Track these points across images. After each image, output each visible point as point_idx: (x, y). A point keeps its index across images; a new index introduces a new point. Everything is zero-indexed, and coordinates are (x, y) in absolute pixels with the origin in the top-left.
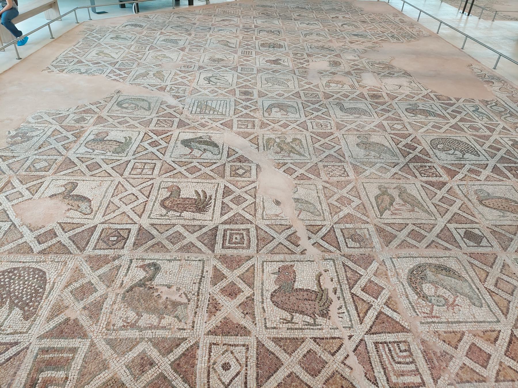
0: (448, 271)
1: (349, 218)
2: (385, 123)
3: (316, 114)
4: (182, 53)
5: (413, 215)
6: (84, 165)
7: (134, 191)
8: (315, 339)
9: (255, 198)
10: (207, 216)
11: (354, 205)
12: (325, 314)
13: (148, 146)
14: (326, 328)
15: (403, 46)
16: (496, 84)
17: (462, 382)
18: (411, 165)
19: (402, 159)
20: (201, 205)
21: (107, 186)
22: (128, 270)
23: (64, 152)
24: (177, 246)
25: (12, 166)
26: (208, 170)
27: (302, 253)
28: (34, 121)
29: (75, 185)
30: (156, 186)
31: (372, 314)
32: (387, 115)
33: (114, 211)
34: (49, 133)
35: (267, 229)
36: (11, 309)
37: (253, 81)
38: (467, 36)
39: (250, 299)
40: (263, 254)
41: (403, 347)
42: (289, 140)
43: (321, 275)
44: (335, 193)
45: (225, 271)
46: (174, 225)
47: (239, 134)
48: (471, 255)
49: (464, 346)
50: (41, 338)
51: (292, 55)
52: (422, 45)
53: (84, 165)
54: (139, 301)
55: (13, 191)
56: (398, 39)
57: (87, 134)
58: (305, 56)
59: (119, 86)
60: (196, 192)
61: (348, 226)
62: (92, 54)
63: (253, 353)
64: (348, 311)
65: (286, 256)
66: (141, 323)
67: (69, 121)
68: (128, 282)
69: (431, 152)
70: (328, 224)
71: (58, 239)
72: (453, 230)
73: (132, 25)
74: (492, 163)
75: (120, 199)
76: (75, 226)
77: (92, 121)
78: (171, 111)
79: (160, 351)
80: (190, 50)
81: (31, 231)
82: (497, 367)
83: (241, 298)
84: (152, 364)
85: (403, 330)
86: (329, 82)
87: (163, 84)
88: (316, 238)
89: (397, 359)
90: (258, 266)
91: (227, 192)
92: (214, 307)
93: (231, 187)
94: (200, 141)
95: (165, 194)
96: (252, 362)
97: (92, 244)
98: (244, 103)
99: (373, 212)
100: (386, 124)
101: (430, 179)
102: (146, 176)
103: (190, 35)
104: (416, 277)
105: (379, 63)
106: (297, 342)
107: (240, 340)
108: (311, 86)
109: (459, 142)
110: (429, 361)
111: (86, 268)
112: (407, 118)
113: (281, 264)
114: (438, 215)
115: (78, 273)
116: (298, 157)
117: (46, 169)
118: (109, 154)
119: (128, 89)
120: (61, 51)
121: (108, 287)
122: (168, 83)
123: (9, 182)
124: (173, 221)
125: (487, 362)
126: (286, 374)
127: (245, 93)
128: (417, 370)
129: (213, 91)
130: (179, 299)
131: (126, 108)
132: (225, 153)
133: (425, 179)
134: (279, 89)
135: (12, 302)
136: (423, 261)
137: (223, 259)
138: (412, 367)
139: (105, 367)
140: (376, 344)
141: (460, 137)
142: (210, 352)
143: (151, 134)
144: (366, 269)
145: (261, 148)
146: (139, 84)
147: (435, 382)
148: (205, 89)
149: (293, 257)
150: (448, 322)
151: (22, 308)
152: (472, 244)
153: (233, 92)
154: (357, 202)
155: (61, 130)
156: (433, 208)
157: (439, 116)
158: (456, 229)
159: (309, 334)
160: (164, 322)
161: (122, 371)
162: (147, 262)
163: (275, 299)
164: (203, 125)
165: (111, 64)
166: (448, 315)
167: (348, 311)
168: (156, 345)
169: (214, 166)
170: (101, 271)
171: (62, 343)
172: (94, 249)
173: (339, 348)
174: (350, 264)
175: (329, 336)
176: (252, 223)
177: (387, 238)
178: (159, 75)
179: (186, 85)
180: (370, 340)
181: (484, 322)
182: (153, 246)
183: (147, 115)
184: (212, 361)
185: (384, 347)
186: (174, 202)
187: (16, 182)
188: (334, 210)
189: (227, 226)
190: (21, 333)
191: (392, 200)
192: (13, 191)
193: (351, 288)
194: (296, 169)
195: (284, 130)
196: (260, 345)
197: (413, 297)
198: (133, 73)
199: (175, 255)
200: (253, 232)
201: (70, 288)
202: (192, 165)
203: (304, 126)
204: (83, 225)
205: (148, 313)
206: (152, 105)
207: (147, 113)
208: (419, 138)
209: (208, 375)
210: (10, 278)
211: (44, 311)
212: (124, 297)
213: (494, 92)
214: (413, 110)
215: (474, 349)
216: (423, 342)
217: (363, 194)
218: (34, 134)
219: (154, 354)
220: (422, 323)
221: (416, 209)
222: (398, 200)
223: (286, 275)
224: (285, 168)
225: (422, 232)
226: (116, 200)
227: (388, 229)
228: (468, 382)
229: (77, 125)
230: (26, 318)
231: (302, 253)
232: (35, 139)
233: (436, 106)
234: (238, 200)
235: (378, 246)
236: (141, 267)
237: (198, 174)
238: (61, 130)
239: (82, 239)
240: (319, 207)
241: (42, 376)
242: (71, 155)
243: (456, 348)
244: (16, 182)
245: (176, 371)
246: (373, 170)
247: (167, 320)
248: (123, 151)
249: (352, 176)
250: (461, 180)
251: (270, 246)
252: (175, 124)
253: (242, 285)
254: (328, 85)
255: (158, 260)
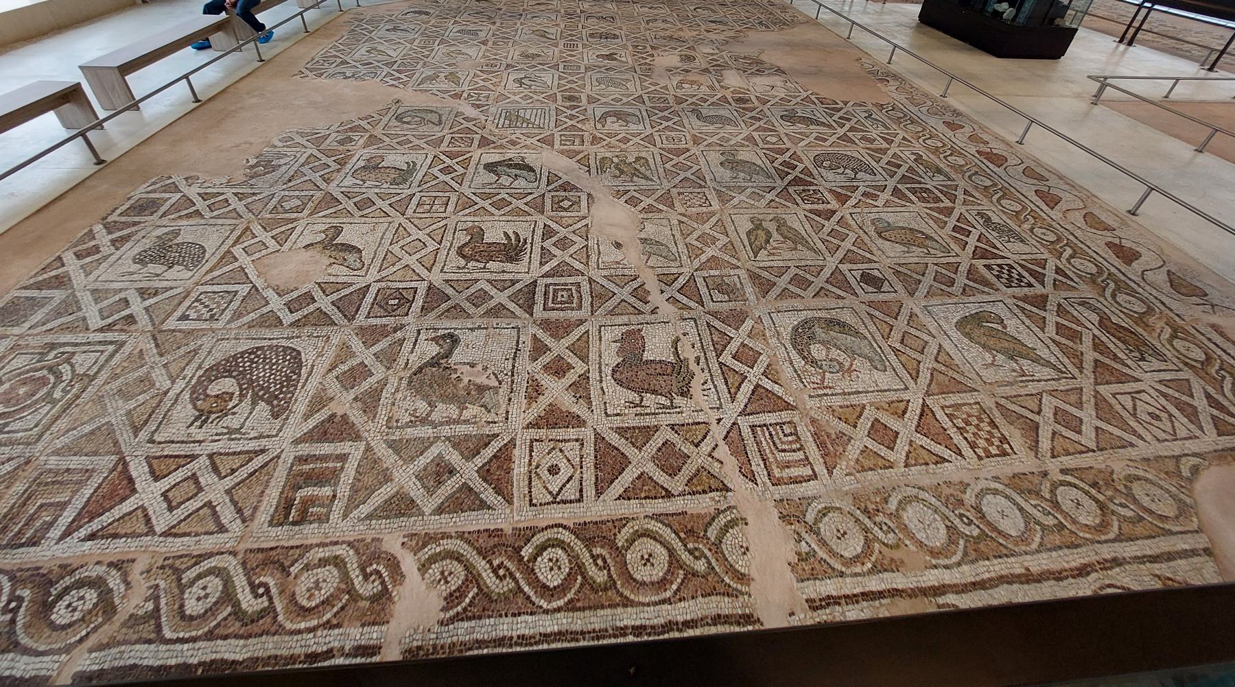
0: (842, 326)
1: (713, 262)
2: (756, 134)
3: (665, 124)
4: (484, 48)
5: (796, 255)
6: (351, 202)
7: (421, 235)
8: (672, 426)
9: (587, 240)
10: (522, 266)
11: (719, 244)
12: (685, 393)
13: (438, 174)
14: (686, 410)
15: (774, 36)
16: (892, 82)
17: (864, 470)
18: (791, 190)
19: (779, 181)
20: (512, 251)
21: (383, 230)
22: (415, 345)
23: (323, 185)
24: (482, 310)
25: (251, 207)
26: (520, 204)
27: (653, 312)
28: (281, 144)
29: (338, 231)
30: (451, 227)
31: (747, 388)
32: (758, 124)
33: (393, 265)
34: (302, 160)
35: (605, 282)
36: (254, 403)
37: (580, 82)
38: (854, 23)
39: (585, 377)
40: (601, 316)
41: (787, 430)
42: (631, 159)
43: (678, 340)
44: (695, 229)
45: (549, 341)
46: (477, 281)
47: (562, 152)
48: (870, 304)
49: (865, 424)
50: (297, 442)
51: (631, 48)
52: (797, 34)
53: (351, 202)
54: (431, 386)
55: (253, 241)
56: (767, 27)
57: (354, 159)
58: (649, 49)
59: (399, 93)
60: (505, 233)
61: (712, 272)
62: (362, 52)
63: (589, 449)
64: (715, 387)
65: (632, 317)
66: (435, 417)
67: (330, 143)
68: (415, 361)
69: (815, 172)
70: (686, 270)
71: (316, 305)
72: (846, 272)
73: (415, 12)
74: (891, 183)
75: (402, 248)
76: (340, 286)
77: (362, 141)
78: (470, 125)
79: (462, 454)
80: (494, 43)
81: (280, 296)
82: (906, 448)
83: (571, 377)
84: (452, 472)
85: (788, 407)
86: (681, 82)
87: (458, 90)
88: (672, 291)
89: (779, 446)
90: (594, 331)
91: (548, 233)
92: (535, 391)
93: (554, 226)
94: (509, 164)
95: (463, 238)
96: (589, 462)
97: (364, 310)
98: (569, 112)
99: (745, 253)
100: (757, 137)
101: (816, 206)
102: (436, 215)
103: (494, 23)
104: (802, 337)
105: (745, 58)
106: (648, 432)
107: (572, 433)
108: (657, 88)
109: (850, 158)
110: (821, 445)
111: (356, 344)
112: (784, 128)
113: (624, 329)
114: (827, 254)
115: (345, 351)
116: (643, 182)
117: (298, 210)
118: (385, 186)
119: (411, 98)
120: (317, 49)
121: (388, 369)
122: (465, 87)
123: (248, 228)
124: (475, 276)
125: (895, 442)
126: (635, 475)
127: (570, 98)
128: (807, 458)
129: (525, 97)
130: (486, 382)
131: (408, 123)
132: (544, 179)
133: (808, 207)
134: (615, 92)
135: (255, 395)
136: (810, 314)
137: (545, 324)
138: (800, 455)
139: (388, 479)
140: (753, 427)
141: (849, 151)
142: (531, 451)
143: (443, 157)
144: (737, 329)
145: (593, 171)
146: (426, 91)
147: (830, 473)
148: (515, 94)
149: (640, 317)
150: (844, 394)
151: (269, 403)
152: (870, 289)
153: (553, 97)
154: (723, 240)
155: (319, 155)
156: (820, 245)
157: (823, 124)
158: (1114, 395)
159: (665, 419)
160: (466, 414)
161: (411, 483)
162: (441, 333)
163: (617, 375)
164: (513, 143)
165: (386, 65)
166: (845, 385)
167: (715, 387)
168: (456, 446)
169: (529, 198)
170: (377, 348)
171: (326, 448)
172: (368, 317)
173: (705, 437)
174: (717, 324)
175: (691, 421)
176: (583, 274)
177: (764, 287)
178: (452, 77)
179: (490, 90)
180: (744, 423)
181: (889, 390)
182: (448, 311)
183: (437, 132)
184: (534, 464)
185: (763, 431)
186: (476, 249)
187: (257, 229)
188: (694, 252)
189: (550, 280)
190: (268, 436)
191: (769, 235)
192: (253, 241)
193: (718, 356)
194: (642, 198)
195: (623, 146)
196: (599, 438)
197: (799, 362)
198: (417, 75)
199: (479, 322)
200: (585, 287)
201: (335, 373)
202: (499, 197)
203: (650, 139)
204: (351, 284)
205: (443, 402)
206: (444, 118)
207: (437, 128)
208: (799, 153)
209: (530, 483)
210: (252, 361)
211: (300, 405)
212: (410, 382)
213: (890, 93)
214: (790, 117)
215: (878, 426)
216: (813, 421)
217: (731, 229)
218: (282, 161)
219: (454, 458)
220: (810, 396)
221: (799, 247)
222: (775, 235)
223: (631, 343)
224: (626, 197)
225: (808, 276)
226: (396, 249)
227: (765, 274)
228: (871, 469)
229: (341, 148)
230: (276, 416)
231: (653, 312)
232: (283, 169)
233: (820, 113)
234: (563, 244)
235: (752, 298)
236: (433, 339)
237: (508, 209)
238: (319, 155)
239: (350, 303)
240: (674, 250)
241: (300, 494)
242: (333, 188)
243: (855, 427)
244: (257, 229)
245: (485, 480)
246: (742, 197)
247: (472, 410)
248: (405, 181)
249: (716, 205)
250: (854, 206)
251: (610, 304)
252: (476, 142)
253: (572, 360)
254: (680, 85)
255: (455, 329)
